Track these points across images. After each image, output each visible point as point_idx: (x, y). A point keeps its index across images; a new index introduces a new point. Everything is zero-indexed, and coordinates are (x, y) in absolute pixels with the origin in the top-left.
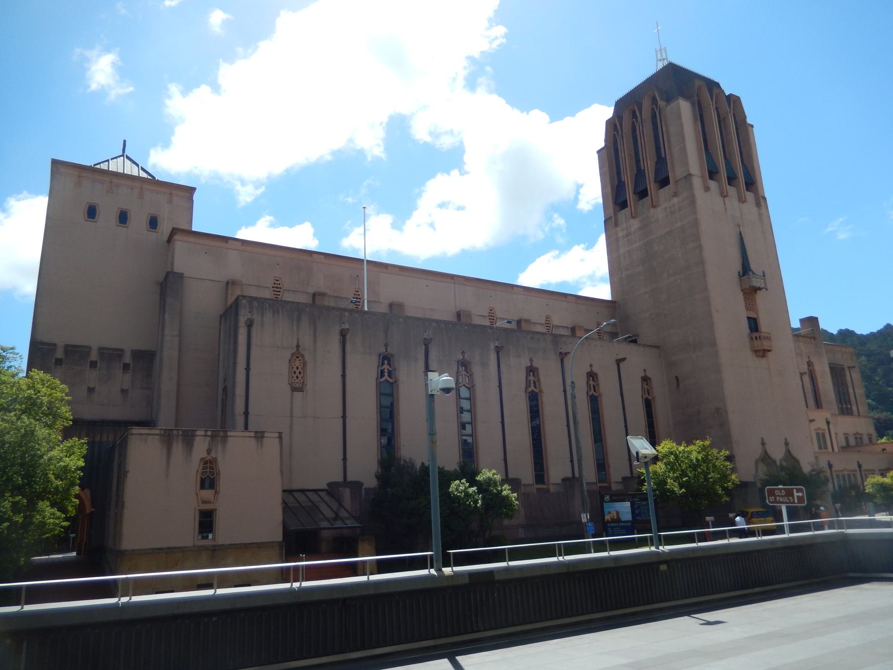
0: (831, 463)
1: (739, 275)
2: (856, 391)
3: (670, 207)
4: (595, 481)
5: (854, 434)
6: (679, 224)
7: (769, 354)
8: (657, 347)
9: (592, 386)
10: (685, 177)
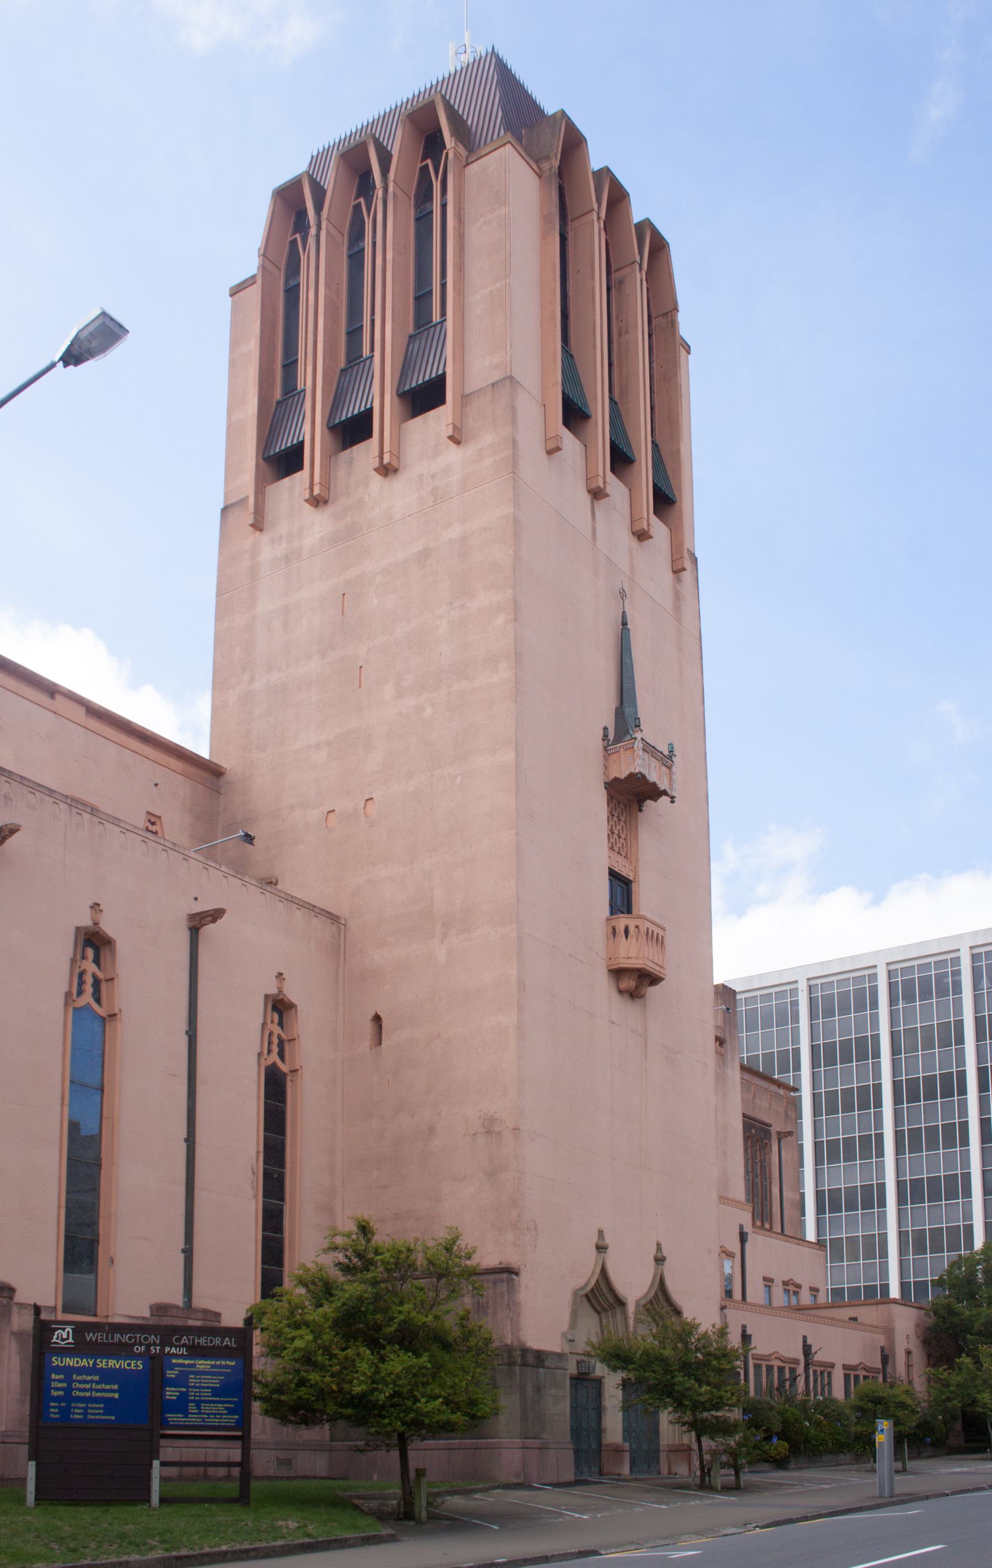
0: (749, 1332)
1: (605, 737)
2: (785, 1194)
3: (433, 476)
4: (52, 1304)
5: (785, 1283)
6: (455, 532)
7: (653, 992)
8: (334, 918)
9: (89, 980)
10: (493, 384)
